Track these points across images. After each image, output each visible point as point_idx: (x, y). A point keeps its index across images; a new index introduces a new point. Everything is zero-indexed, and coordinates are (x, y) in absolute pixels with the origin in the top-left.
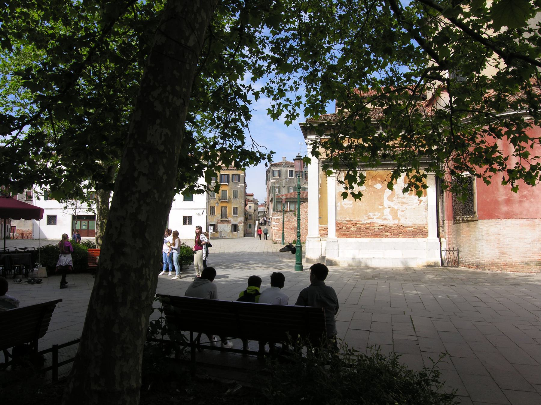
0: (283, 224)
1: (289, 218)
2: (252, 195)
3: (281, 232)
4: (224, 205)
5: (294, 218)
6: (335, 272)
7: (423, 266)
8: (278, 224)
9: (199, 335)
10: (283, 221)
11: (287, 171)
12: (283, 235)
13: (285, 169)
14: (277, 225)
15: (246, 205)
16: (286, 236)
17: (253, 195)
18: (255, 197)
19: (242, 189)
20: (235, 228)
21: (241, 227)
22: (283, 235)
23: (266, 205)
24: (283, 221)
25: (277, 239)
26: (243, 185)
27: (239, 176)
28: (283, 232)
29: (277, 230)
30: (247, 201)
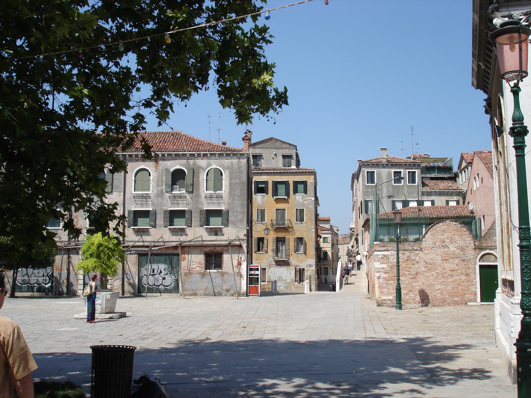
0: (398, 266)
1: (407, 253)
2: (327, 221)
3: (394, 283)
4: (281, 235)
5: (417, 254)
6: (181, 343)
7: (455, 360)
8: (385, 266)
9: (314, 177)
10: (398, 262)
11: (389, 174)
12: (399, 290)
13: (387, 170)
14: (383, 268)
15: (318, 236)
16: (403, 292)
17: (329, 220)
18: (332, 223)
19: (312, 207)
20: (300, 274)
21: (311, 271)
22: (399, 290)
23: (352, 235)
24: (398, 262)
25: (384, 298)
26: (313, 199)
27: (305, 183)
28: (399, 284)
29: (384, 278)
30: (319, 230)
